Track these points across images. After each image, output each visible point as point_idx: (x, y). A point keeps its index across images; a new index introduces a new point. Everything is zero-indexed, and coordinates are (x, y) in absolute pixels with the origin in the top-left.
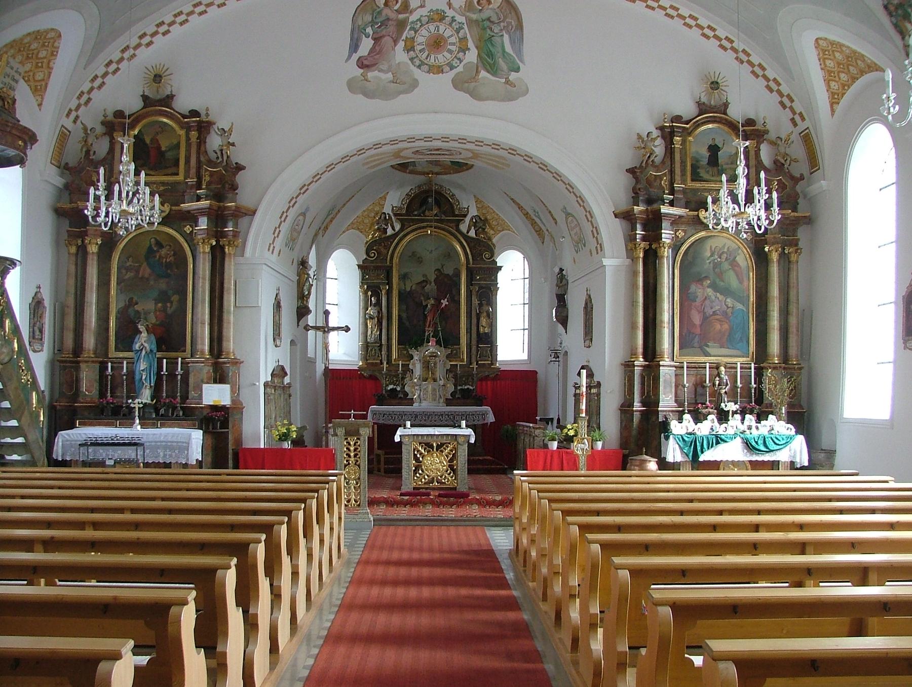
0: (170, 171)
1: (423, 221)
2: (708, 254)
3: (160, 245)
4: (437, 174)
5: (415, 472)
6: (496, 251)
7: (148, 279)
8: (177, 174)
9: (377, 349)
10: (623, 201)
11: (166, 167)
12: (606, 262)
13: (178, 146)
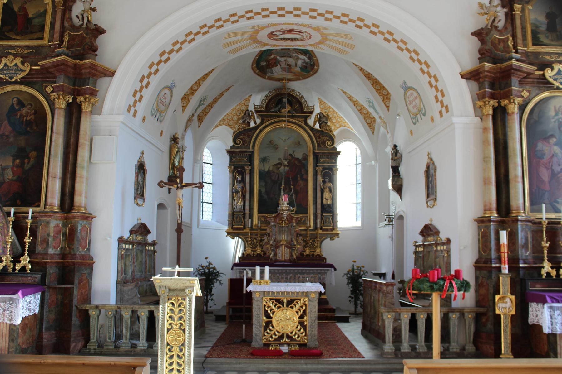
0: (35, 36)
1: (279, 116)
2: (552, 113)
3: (21, 104)
4: (290, 80)
5: (266, 328)
6: (336, 140)
7: (8, 137)
8: (42, 39)
9: (241, 217)
10: (470, 61)
11: (32, 33)
12: (455, 120)
13: (44, 13)
